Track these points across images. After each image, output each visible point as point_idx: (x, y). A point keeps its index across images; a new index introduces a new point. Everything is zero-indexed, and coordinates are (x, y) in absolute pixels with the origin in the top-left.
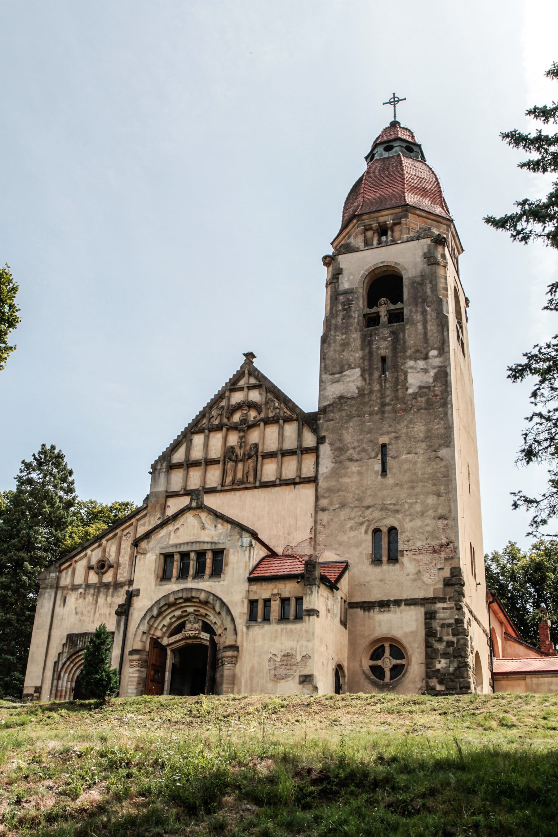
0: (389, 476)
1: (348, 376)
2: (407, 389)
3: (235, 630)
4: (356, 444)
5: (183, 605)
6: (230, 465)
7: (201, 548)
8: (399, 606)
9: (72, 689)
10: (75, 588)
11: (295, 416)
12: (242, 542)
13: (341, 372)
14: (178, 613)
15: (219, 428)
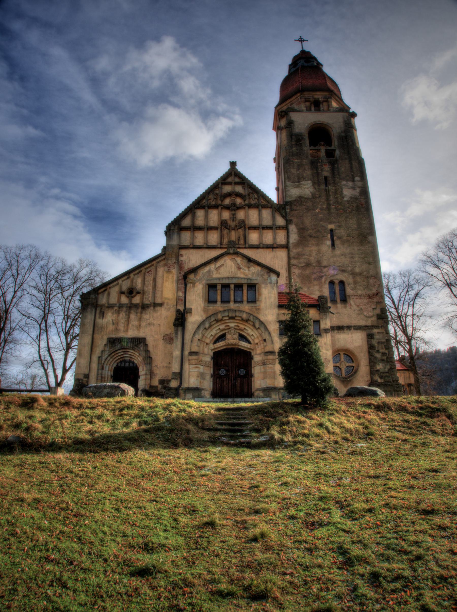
0: (336, 249)
1: (304, 185)
2: (343, 197)
3: (272, 340)
4: (313, 227)
5: (227, 321)
6: (226, 232)
7: (240, 282)
8: (350, 330)
9: (112, 376)
10: (110, 307)
11: (269, 205)
12: (271, 280)
13: (299, 182)
14: (222, 327)
15: (216, 207)
